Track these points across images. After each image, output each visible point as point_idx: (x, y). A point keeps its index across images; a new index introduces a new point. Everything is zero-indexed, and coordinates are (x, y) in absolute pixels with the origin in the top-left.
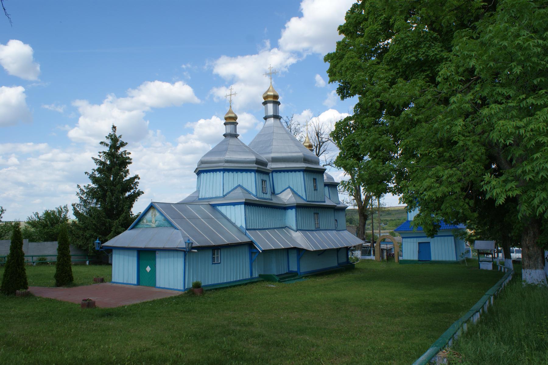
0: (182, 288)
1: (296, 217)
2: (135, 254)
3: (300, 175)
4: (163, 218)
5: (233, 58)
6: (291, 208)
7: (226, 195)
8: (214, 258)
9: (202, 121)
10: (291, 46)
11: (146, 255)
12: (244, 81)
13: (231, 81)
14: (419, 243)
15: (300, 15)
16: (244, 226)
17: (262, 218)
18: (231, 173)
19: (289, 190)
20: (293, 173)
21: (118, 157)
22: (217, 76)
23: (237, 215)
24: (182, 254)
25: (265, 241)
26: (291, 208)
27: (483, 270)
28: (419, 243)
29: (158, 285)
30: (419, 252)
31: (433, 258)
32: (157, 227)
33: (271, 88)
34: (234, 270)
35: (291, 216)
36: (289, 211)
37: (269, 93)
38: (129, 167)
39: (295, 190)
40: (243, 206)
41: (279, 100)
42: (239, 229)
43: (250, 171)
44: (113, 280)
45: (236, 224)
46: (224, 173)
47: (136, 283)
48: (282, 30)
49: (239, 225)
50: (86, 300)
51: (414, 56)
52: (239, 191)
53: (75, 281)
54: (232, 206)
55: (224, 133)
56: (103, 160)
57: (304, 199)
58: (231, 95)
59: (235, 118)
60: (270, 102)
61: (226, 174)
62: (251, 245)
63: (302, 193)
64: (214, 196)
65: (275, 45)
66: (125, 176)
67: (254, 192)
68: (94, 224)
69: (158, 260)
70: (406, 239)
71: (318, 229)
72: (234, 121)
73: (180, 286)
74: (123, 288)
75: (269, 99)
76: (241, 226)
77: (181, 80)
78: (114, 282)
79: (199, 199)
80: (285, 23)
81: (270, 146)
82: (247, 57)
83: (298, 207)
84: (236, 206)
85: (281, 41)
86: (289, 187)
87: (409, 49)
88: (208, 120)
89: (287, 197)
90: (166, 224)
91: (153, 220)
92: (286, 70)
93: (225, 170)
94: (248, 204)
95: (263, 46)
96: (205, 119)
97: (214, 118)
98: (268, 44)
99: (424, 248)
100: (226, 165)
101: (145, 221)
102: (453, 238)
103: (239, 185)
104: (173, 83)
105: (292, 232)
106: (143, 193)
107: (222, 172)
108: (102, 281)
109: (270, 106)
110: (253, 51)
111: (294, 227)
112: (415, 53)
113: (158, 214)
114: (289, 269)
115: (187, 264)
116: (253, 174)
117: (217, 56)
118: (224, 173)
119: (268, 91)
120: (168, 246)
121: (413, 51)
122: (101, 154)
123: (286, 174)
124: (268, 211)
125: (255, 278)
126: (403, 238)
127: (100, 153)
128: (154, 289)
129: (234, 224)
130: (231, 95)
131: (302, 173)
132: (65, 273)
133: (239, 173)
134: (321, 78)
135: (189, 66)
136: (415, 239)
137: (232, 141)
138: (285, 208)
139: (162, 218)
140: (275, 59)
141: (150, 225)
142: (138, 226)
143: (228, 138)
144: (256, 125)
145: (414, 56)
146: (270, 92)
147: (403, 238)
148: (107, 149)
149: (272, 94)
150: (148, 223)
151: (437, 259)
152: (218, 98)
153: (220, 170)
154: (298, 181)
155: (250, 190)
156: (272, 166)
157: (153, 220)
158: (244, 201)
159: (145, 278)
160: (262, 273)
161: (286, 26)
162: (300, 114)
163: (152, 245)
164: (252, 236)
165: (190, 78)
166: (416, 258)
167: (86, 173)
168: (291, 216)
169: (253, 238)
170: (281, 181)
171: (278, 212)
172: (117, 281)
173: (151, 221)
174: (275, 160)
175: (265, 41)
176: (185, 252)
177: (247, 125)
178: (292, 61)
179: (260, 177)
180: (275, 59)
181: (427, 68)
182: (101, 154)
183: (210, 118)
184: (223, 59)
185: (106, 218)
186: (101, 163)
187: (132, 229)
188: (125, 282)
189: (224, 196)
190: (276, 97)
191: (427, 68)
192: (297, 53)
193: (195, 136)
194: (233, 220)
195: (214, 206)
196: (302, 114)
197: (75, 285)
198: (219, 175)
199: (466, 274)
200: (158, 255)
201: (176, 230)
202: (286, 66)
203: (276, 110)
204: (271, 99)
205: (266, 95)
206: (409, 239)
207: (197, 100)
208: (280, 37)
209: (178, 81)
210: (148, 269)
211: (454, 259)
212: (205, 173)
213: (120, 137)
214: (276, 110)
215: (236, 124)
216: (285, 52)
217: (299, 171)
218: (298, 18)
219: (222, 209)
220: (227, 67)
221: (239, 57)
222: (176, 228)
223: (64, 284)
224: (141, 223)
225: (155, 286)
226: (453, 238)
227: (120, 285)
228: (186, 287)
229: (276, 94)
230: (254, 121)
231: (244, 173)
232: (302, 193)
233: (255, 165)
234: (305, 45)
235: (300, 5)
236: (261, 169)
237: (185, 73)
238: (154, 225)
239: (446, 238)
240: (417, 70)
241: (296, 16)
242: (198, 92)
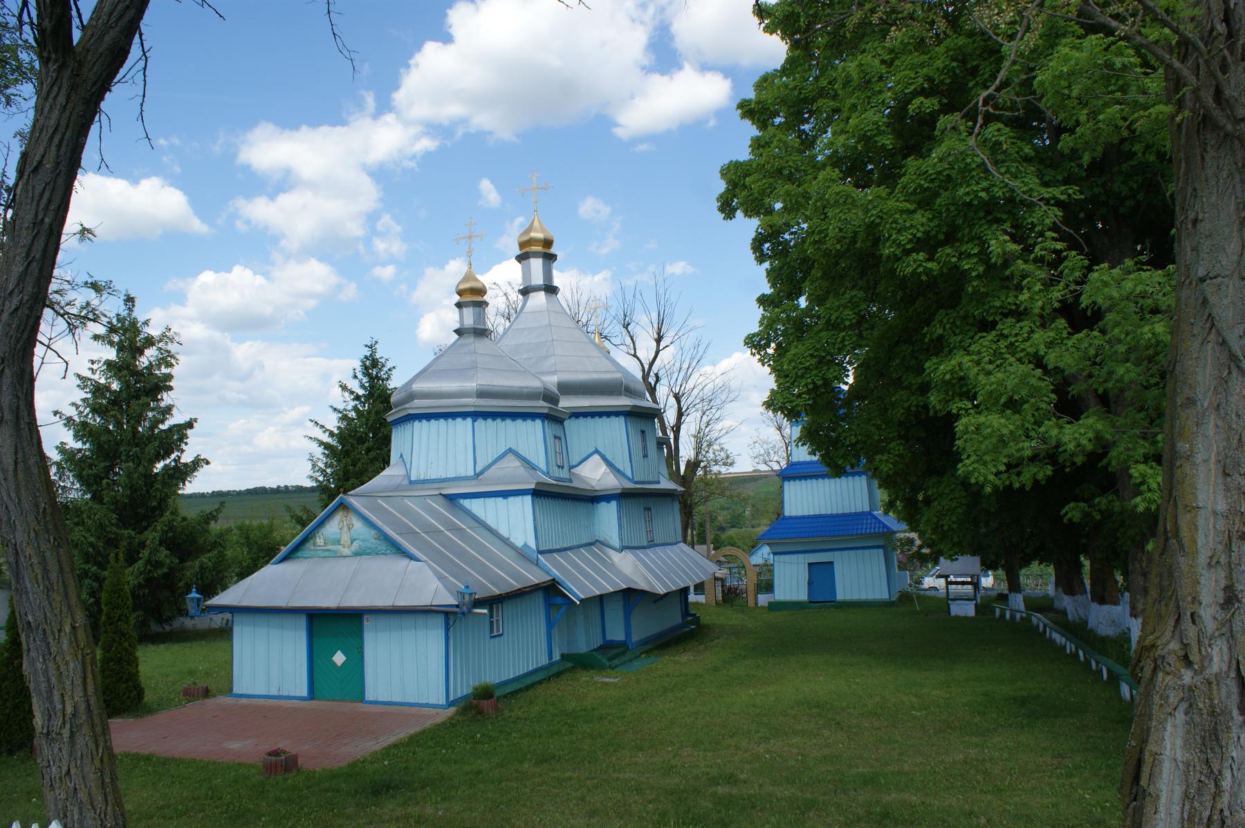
0: (442, 701)
1: (619, 519)
2: (302, 622)
3: (619, 424)
4: (373, 532)
5: (287, 133)
6: (607, 498)
7: (482, 473)
8: (492, 623)
9: (207, 277)
10: (422, 111)
11: (334, 626)
12: (311, 185)
13: (279, 184)
14: (810, 564)
15: (447, 39)
16: (532, 544)
17: (565, 526)
18: (490, 421)
19: (596, 457)
20: (604, 418)
21: (137, 374)
22: (247, 168)
23: (516, 521)
24: (440, 620)
25: (583, 581)
26: (607, 498)
27: (957, 618)
28: (810, 564)
29: (370, 695)
30: (810, 583)
31: (840, 596)
32: (356, 554)
33: (536, 224)
34: (521, 651)
35: (608, 518)
36: (603, 504)
37: (533, 235)
38: (167, 398)
39: (609, 457)
40: (529, 498)
41: (553, 250)
42: (522, 553)
43: (532, 416)
44: (236, 690)
45: (512, 540)
46: (474, 421)
47: (305, 693)
48: (402, 70)
49: (519, 543)
50: (275, 753)
51: (983, 190)
52: (512, 464)
53: (148, 697)
54: (500, 500)
55: (457, 326)
56: (103, 381)
57: (628, 478)
58: (470, 237)
59: (481, 291)
60: (536, 255)
61: (480, 423)
62: (551, 590)
63: (624, 464)
64: (451, 475)
65: (384, 106)
66: (163, 422)
67: (543, 465)
68: (91, 544)
69: (369, 637)
70: (782, 557)
71: (652, 544)
72: (480, 299)
73: (437, 696)
74: (266, 711)
75: (534, 248)
76: (526, 545)
77: (156, 175)
78: (241, 696)
79: (411, 482)
80: (411, 56)
81: (548, 357)
82: (324, 129)
83: (624, 496)
84: (511, 499)
85: (399, 97)
86: (597, 452)
87: (974, 173)
88: (223, 275)
89: (595, 474)
90: (383, 546)
91: (345, 538)
92: (413, 164)
93: (476, 415)
94: (540, 493)
95: (360, 105)
96: (216, 272)
97: (238, 270)
98: (370, 101)
99: (820, 575)
100: (482, 402)
101: (320, 541)
102: (881, 551)
103: (510, 450)
104: (135, 181)
105: (616, 557)
106: (208, 463)
107: (469, 420)
108: (206, 693)
109: (537, 264)
110: (337, 119)
111: (616, 542)
112: (985, 184)
113: (358, 525)
114: (604, 636)
115: (451, 642)
116: (538, 422)
117: (249, 122)
118: (474, 421)
119: (530, 229)
120: (403, 602)
121: (980, 178)
122: (95, 367)
123: (589, 420)
124: (569, 505)
125: (557, 662)
126: (774, 554)
127: (93, 362)
128: (361, 707)
129: (506, 541)
130: (470, 237)
131: (622, 419)
132: (127, 681)
133: (508, 421)
134: (492, 187)
135: (176, 141)
136: (801, 556)
137: (481, 345)
138: (592, 498)
139: (368, 534)
140: (386, 138)
141: (335, 552)
142: (299, 554)
143: (469, 340)
144: (339, 288)
145: (983, 190)
146: (536, 231)
147: (774, 554)
148: (111, 354)
149: (540, 236)
150: (330, 547)
151: (848, 597)
152: (248, 222)
153: (464, 415)
154: (614, 434)
155: (533, 460)
156: (566, 403)
157: (345, 538)
158: (533, 486)
159: (336, 684)
160: (566, 652)
161: (412, 62)
162: (442, 268)
163: (355, 600)
164: (552, 569)
165: (179, 170)
166: (803, 596)
167: (56, 413)
168: (608, 518)
169: (556, 573)
170: (581, 434)
171: (582, 508)
172: (250, 692)
173: (338, 542)
174: (568, 389)
175: (362, 92)
176: (446, 614)
177: (319, 288)
178: (426, 144)
179: (551, 429)
180: (386, 138)
181: (1004, 216)
182: (95, 367)
183: (229, 270)
184: (264, 131)
185: (117, 526)
186: (98, 390)
187: (285, 559)
188: (274, 692)
189: (477, 475)
190: (548, 243)
191: (1004, 216)
192: (432, 128)
193: (189, 311)
194: (504, 532)
195: (452, 499)
196: (447, 267)
197: (150, 711)
198: (463, 427)
199: (991, 630)
200: (368, 623)
201: (413, 562)
202: (414, 157)
203: (548, 274)
204: (539, 249)
205: (525, 238)
206: (788, 557)
207: (198, 226)
208: (396, 86)
209: (147, 176)
210: (339, 658)
211: (885, 596)
212: (424, 421)
213: (146, 323)
214: (548, 274)
215: (483, 305)
216: (407, 123)
217: (617, 414)
218: (440, 44)
219: (475, 506)
220: (269, 150)
221: (304, 127)
222: (412, 557)
223: (124, 711)
224: (309, 545)
225: (361, 698)
226: (881, 551)
227: (393, 708)
228: (451, 698)
229: (549, 236)
230: (334, 279)
231: (519, 421)
232: (624, 464)
233: (542, 403)
234: (455, 110)
235: (446, 15)
236: (549, 411)
237: (165, 159)
238: (346, 551)
239: (867, 552)
240: (980, 219)
241: (436, 40)
242: (199, 205)
